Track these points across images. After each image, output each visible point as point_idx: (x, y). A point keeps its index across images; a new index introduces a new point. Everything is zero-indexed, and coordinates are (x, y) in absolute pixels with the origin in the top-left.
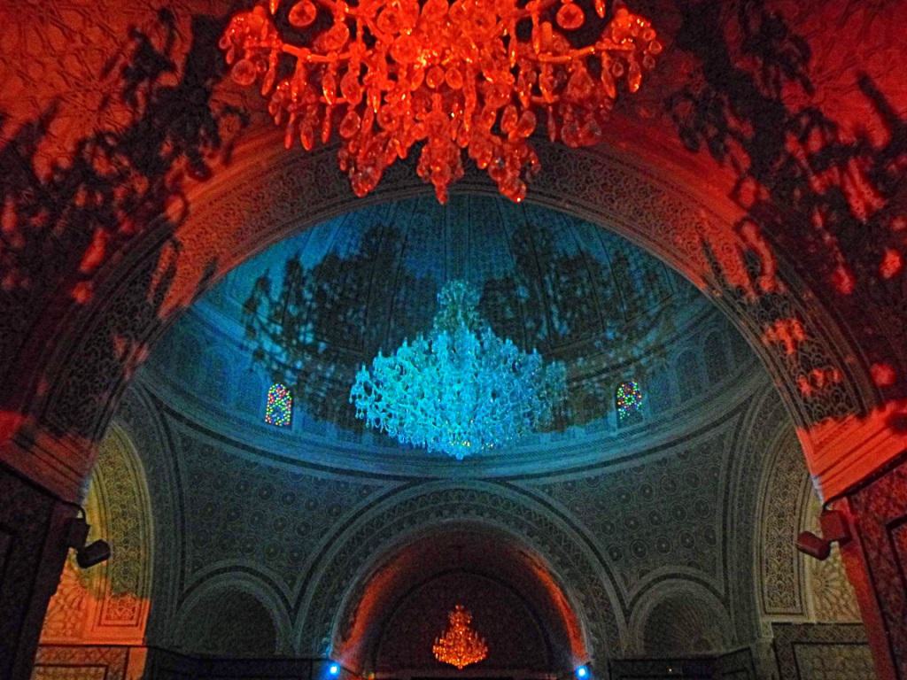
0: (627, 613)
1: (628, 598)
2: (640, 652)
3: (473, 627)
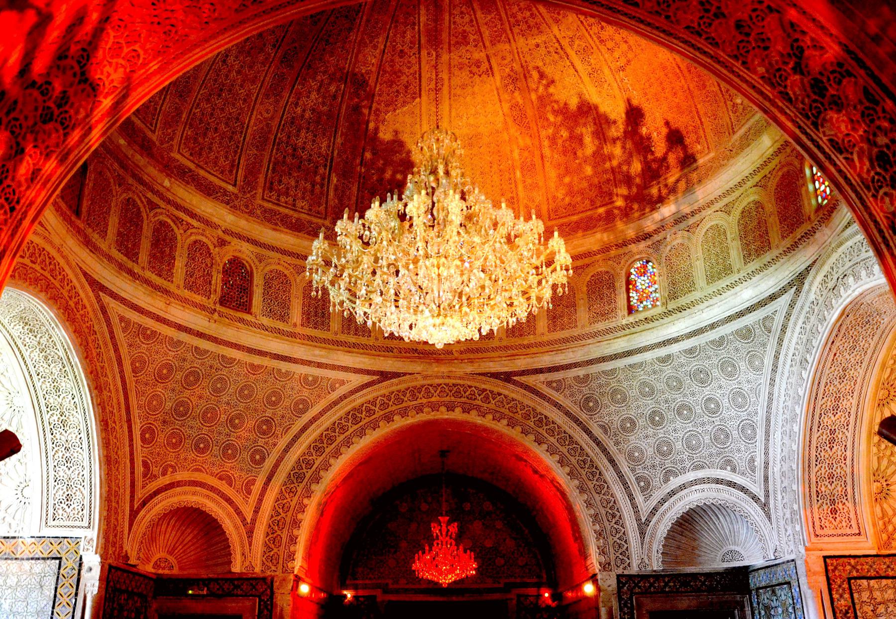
1: (645, 508)
2: (656, 565)
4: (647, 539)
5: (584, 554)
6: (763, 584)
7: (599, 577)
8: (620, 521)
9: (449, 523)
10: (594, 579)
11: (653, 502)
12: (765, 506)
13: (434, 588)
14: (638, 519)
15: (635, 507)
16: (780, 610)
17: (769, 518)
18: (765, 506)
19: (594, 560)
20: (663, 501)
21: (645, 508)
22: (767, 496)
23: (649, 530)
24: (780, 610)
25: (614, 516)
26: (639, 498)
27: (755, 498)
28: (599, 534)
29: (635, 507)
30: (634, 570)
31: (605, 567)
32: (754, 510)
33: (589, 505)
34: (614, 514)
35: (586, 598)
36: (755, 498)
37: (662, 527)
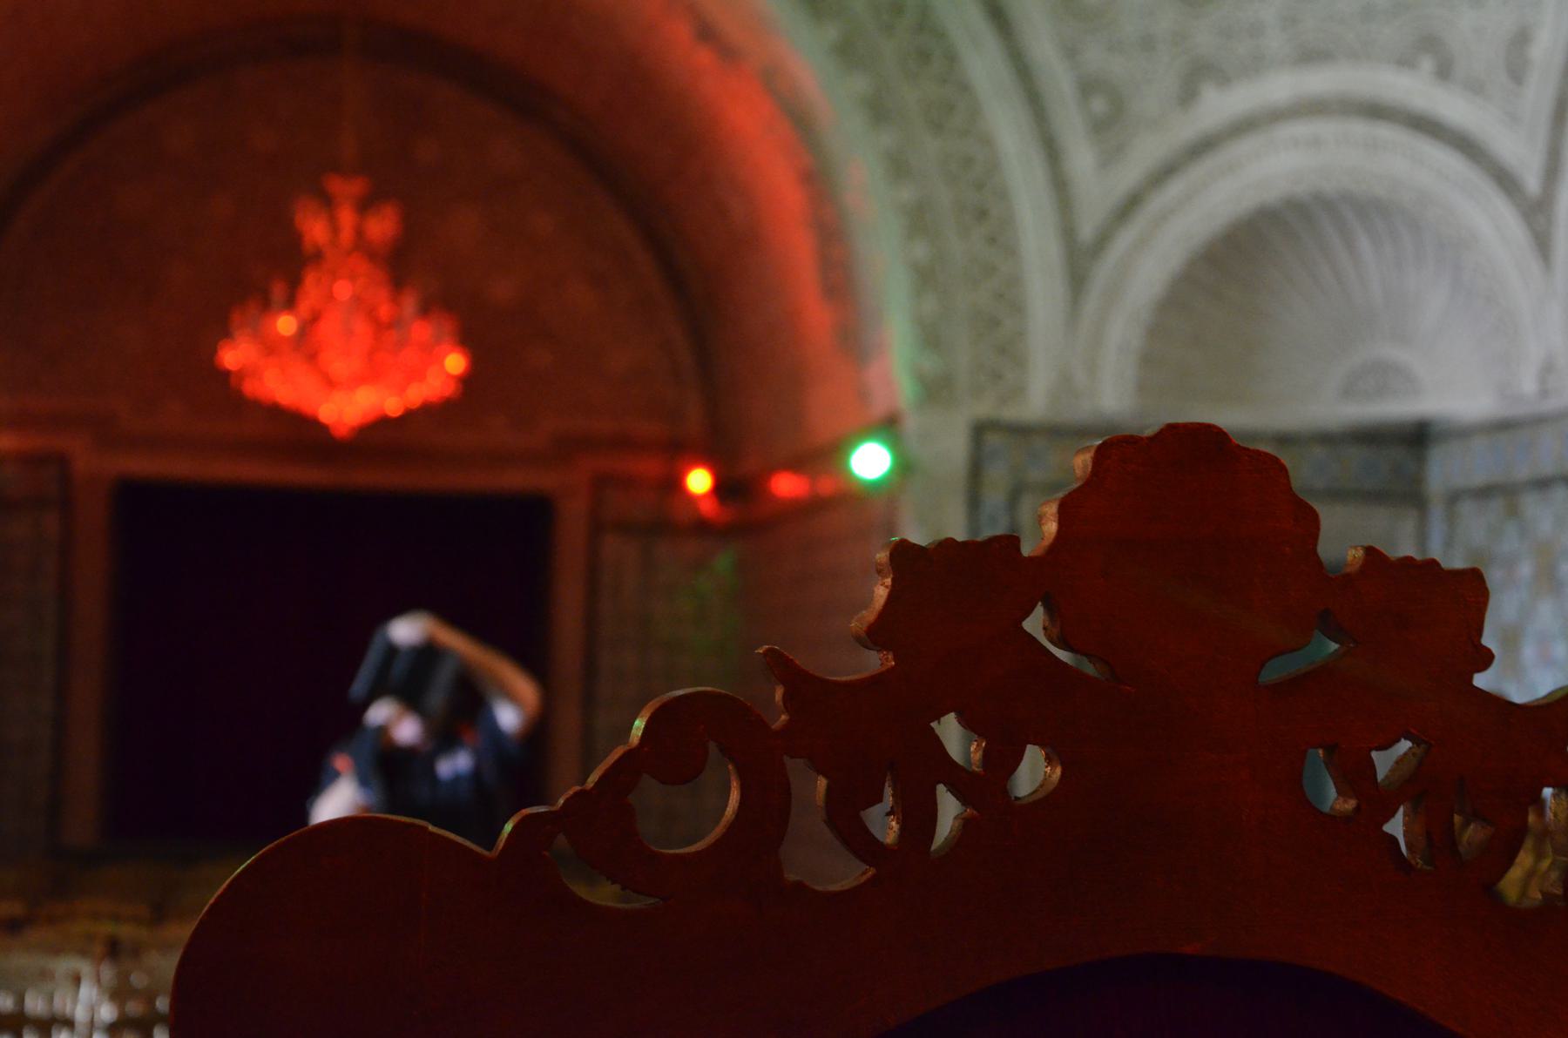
0: (1079, 262)
1: (1097, 185)
3: (398, 265)
4: (1092, 302)
5: (853, 341)
6: (1479, 479)
7: (911, 423)
8: (1002, 238)
9: (365, 205)
10: (888, 427)
11: (1129, 174)
12: (1538, 214)
13: (300, 433)
14: (1068, 232)
15: (1060, 185)
16: (1525, 570)
17: (1543, 244)
18: (1538, 214)
19: (897, 363)
20: (1166, 172)
21: (1097, 185)
22: (1551, 173)
23: (1102, 272)
24: (1525, 570)
25: (982, 214)
26: (1081, 158)
27: (1505, 180)
28: (925, 277)
29: (1060, 185)
30: (1036, 404)
31: (936, 390)
32: (1492, 224)
33: (898, 167)
34: (985, 210)
35: (855, 497)
36: (1505, 180)
37: (1150, 264)
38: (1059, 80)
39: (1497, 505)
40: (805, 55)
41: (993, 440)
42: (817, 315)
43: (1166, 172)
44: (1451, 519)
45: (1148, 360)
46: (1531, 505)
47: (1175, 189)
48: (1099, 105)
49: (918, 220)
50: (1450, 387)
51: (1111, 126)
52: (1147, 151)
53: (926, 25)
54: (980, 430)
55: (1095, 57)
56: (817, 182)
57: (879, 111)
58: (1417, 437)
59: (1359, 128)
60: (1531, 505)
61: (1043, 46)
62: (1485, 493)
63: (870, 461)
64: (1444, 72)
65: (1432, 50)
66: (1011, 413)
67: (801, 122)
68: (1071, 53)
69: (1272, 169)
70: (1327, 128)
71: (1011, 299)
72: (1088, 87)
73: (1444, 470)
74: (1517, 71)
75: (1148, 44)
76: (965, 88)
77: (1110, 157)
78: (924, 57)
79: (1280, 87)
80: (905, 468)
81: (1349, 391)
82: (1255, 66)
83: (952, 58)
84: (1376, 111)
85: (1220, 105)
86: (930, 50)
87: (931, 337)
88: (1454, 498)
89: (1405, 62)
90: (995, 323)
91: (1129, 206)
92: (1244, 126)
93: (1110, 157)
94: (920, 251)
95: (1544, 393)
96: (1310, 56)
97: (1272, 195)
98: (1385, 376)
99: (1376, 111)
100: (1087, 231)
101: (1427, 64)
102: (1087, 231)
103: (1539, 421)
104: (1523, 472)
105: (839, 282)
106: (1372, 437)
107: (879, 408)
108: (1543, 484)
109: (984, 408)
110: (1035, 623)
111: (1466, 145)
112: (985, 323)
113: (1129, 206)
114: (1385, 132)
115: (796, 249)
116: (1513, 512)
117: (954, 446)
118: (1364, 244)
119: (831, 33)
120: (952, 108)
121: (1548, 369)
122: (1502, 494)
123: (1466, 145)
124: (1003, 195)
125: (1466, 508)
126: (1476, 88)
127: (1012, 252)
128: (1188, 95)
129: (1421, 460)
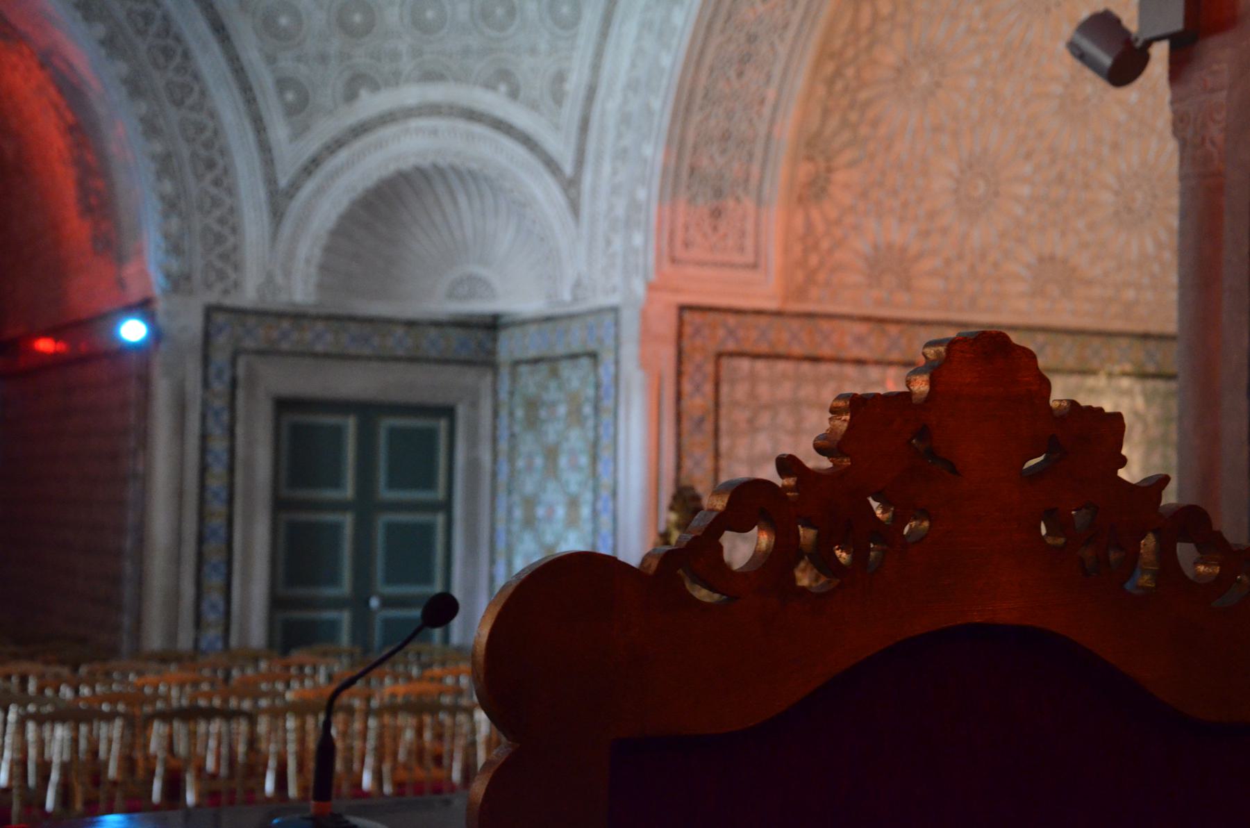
0: (279, 202)
1: (291, 154)
5: (110, 244)
6: (532, 353)
7: (161, 306)
10: (144, 308)
11: (312, 144)
12: (571, 186)
14: (271, 180)
15: (265, 148)
16: (562, 410)
18: (571, 186)
19: (150, 263)
20: (336, 145)
21: (291, 154)
24: (562, 410)
25: (211, 165)
26: (279, 131)
27: (551, 165)
28: (171, 205)
30: (249, 294)
31: (178, 283)
32: (544, 192)
33: (151, 129)
34: (212, 161)
36: (551, 165)
37: (327, 203)
38: (263, 78)
39: (544, 368)
40: (79, 45)
41: (220, 318)
42: (77, 227)
43: (336, 145)
44: (514, 377)
45: (324, 268)
46: (566, 369)
47: (343, 155)
48: (290, 96)
49: (165, 165)
50: (517, 294)
51: (300, 109)
52: (324, 130)
53: (167, 28)
54: (210, 311)
55: (287, 63)
56: (82, 132)
57: (135, 88)
58: (493, 325)
59: (462, 125)
60: (566, 369)
61: (251, 54)
62: (536, 361)
63: (133, 331)
64: (514, 94)
65: (504, 78)
66: (229, 301)
67: (71, 91)
68: (271, 60)
69: (408, 146)
70: (442, 124)
71: (231, 222)
72: (282, 84)
73: (509, 346)
74: (558, 98)
75: (323, 58)
76: (196, 77)
77: (298, 133)
78: (167, 53)
79: (411, 94)
80: (157, 335)
81: (451, 295)
82: (395, 79)
83: (186, 55)
84: (471, 115)
85: (371, 104)
86: (171, 48)
87: (175, 248)
88: (517, 363)
89: (489, 86)
90: (219, 239)
91: (314, 163)
92: (388, 118)
93: (298, 133)
94: (168, 187)
95: (575, 299)
96: (430, 76)
97: (406, 165)
98: (475, 285)
99: (471, 115)
100: (283, 182)
101: (503, 88)
102: (283, 182)
103: (571, 317)
104: (560, 350)
105: (99, 203)
106: (465, 324)
107: (135, 294)
108: (574, 357)
109: (213, 297)
110: (1144, 580)
111: (528, 141)
112: (209, 235)
113: (314, 163)
114: (478, 129)
115: (64, 181)
116: (555, 374)
117: (194, 322)
118: (462, 200)
119: (100, 30)
120: (187, 89)
121: (578, 285)
122: (547, 362)
123: (528, 141)
124: (224, 152)
125: (524, 369)
126: (534, 106)
127: (231, 191)
128: (351, 96)
129: (495, 340)
